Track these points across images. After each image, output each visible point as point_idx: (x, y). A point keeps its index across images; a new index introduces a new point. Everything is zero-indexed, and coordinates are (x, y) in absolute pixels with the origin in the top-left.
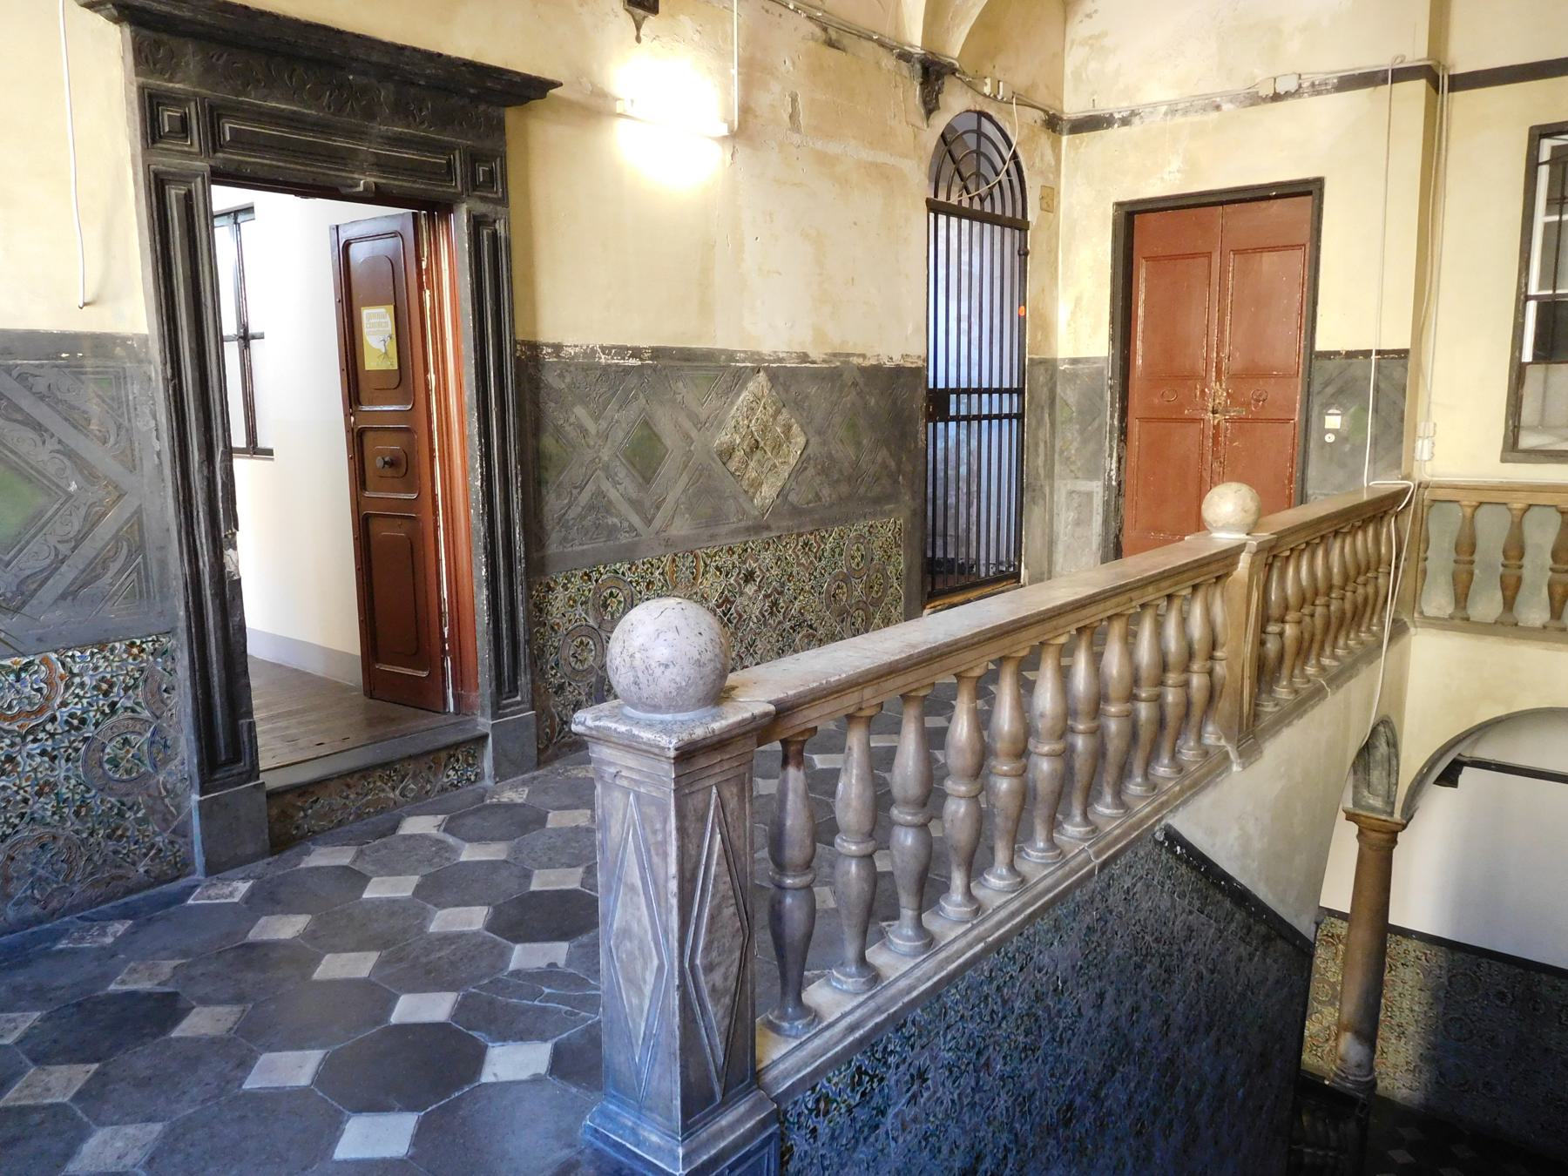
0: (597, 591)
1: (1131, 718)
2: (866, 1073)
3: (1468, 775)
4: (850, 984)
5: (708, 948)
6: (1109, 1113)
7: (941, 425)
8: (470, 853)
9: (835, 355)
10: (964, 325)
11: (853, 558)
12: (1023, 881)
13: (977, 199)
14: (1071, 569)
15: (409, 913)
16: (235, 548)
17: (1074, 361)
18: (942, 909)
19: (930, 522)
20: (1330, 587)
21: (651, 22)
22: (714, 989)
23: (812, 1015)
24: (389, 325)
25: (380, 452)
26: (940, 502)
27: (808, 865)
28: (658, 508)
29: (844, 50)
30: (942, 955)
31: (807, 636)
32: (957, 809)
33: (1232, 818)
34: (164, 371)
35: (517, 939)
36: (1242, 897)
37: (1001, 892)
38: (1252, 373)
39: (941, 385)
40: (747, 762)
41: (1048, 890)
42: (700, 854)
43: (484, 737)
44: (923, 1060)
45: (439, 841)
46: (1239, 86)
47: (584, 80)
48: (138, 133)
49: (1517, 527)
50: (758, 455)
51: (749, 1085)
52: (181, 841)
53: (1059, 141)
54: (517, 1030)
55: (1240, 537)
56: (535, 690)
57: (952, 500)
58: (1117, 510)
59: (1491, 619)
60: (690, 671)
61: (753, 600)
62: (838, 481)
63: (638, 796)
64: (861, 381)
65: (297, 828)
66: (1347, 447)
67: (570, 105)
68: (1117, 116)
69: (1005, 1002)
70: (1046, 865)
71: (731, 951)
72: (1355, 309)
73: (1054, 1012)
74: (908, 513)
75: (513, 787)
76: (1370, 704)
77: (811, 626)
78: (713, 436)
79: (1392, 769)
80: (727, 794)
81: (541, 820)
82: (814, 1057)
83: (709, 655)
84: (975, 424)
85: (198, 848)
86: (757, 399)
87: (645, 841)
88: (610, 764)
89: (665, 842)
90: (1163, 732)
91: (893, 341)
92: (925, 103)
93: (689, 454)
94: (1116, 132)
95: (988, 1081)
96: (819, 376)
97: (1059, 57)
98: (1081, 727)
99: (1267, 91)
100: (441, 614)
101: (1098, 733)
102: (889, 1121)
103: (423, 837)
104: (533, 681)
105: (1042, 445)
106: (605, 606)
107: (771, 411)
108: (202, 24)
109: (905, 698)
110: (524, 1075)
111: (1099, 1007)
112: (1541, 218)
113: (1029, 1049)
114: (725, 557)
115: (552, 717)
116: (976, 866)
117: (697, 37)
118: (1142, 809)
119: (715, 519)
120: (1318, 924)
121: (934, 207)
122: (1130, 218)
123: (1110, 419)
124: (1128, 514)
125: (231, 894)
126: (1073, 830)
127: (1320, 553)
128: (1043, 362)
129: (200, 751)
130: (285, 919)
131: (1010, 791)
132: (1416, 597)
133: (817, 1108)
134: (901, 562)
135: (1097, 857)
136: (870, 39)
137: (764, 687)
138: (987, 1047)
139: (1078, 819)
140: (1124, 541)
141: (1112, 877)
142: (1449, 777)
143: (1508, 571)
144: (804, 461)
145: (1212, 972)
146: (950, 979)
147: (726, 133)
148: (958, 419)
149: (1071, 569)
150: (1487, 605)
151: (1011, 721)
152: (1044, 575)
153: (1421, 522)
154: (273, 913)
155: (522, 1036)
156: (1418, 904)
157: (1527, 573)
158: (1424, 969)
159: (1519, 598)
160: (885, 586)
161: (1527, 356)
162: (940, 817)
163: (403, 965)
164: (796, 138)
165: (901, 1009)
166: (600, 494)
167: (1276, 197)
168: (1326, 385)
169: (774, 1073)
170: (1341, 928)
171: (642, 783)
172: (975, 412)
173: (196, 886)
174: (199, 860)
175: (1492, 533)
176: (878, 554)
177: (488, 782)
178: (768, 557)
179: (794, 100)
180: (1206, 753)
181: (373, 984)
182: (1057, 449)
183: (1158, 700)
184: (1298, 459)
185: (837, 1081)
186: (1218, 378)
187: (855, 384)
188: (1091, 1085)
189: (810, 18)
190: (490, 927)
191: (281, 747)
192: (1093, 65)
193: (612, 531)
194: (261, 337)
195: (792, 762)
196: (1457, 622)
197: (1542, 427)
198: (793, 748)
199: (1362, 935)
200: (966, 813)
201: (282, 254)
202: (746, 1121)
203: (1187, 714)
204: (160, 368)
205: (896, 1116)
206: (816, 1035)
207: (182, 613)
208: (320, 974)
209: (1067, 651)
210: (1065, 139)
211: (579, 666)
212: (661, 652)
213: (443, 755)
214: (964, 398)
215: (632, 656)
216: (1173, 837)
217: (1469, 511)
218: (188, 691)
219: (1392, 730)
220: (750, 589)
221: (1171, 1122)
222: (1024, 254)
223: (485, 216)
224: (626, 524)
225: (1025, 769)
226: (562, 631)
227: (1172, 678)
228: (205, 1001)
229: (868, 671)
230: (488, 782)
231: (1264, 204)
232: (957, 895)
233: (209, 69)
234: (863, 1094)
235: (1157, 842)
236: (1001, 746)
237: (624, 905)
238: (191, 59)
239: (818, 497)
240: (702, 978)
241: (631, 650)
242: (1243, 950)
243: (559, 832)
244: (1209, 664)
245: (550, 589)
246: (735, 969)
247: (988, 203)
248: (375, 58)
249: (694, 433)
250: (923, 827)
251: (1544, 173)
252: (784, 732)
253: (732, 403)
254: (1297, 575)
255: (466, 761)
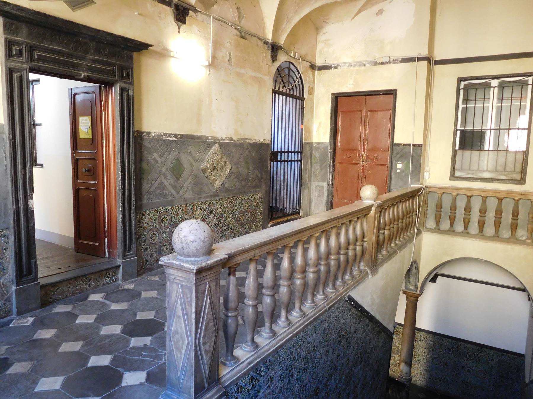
0: (160, 216)
1: (338, 260)
2: (254, 378)
3: (439, 279)
4: (249, 348)
5: (204, 337)
6: (330, 390)
7: (275, 163)
8: (114, 307)
9: (241, 139)
10: (283, 130)
11: (246, 206)
12: (304, 314)
13: (288, 90)
14: (317, 213)
15: (93, 328)
16: (32, 199)
17: (318, 143)
18: (278, 323)
19: (271, 195)
20: (399, 219)
21: (183, 27)
22: (206, 351)
23: (236, 359)
24: (89, 123)
25: (85, 167)
26: (275, 188)
27: (236, 309)
28: (181, 188)
29: (246, 40)
30: (279, 338)
31: (230, 232)
32: (284, 290)
33: (369, 292)
34: (9, 137)
35: (133, 336)
36: (372, 318)
37: (297, 317)
38: (375, 150)
39: (276, 150)
40: (218, 274)
41: (312, 317)
42: (203, 305)
43: (119, 266)
44: (272, 374)
45: (102, 303)
46: (371, 59)
47: (160, 44)
48: (4, 54)
49: (454, 201)
50: (215, 171)
51: (216, 383)
52: (8, 303)
53: (315, 73)
54: (134, 368)
55: (372, 202)
56: (138, 251)
57: (278, 188)
58: (332, 192)
59: (446, 229)
60: (201, 244)
61: (212, 220)
62: (241, 181)
63: (182, 286)
64: (250, 148)
65: (51, 298)
66: (404, 174)
67: (156, 53)
68: (333, 66)
69: (298, 354)
70: (312, 308)
71: (212, 338)
72: (405, 133)
73: (313, 357)
74: (264, 191)
75: (129, 283)
76: (411, 257)
77: (231, 229)
78: (200, 165)
79: (417, 278)
80: (212, 285)
81: (139, 295)
82: (237, 373)
83: (207, 239)
84: (286, 163)
85: (14, 306)
86: (215, 153)
87: (184, 301)
88: (172, 275)
89: (191, 301)
90: (345, 267)
91: (260, 134)
92: (272, 58)
93: (192, 171)
94: (332, 71)
95: (293, 380)
96: (235, 145)
97: (315, 46)
98: (323, 263)
99: (379, 61)
100: (104, 223)
101: (328, 265)
102: (261, 394)
103: (97, 301)
104: (137, 247)
105: (308, 170)
106: (162, 221)
107: (220, 156)
108: (29, 18)
109: (268, 253)
110: (137, 383)
111: (327, 355)
112: (461, 106)
113: (306, 369)
114: (203, 205)
115: (143, 259)
116: (289, 309)
117: (198, 32)
118: (341, 290)
119: (200, 192)
120: (394, 327)
121: (275, 92)
122: (337, 98)
123: (329, 162)
124: (335, 193)
125: (27, 322)
126: (319, 297)
127: (396, 208)
128: (308, 143)
129: (17, 271)
130: (47, 331)
131: (301, 284)
132: (424, 222)
133: (238, 391)
134: (261, 208)
135: (327, 305)
136: (255, 36)
137: (225, 248)
138: (292, 369)
139: (321, 293)
140: (334, 202)
141: (332, 312)
142: (434, 280)
143: (452, 214)
144: (230, 174)
145: (362, 343)
146: (281, 347)
147: (207, 64)
148: (281, 161)
149: (317, 213)
150: (445, 225)
151: (301, 261)
152: (308, 214)
153: (426, 198)
154: (44, 329)
155: (136, 369)
156: (425, 321)
157: (457, 215)
158: (426, 341)
159: (455, 223)
160: (256, 216)
161: (457, 148)
162: (278, 293)
163: (92, 346)
164: (230, 67)
165: (265, 356)
166: (161, 183)
167: (382, 94)
168: (397, 154)
169: (224, 379)
170: (401, 329)
171: (184, 281)
172: (286, 159)
173: (13, 320)
174: (14, 310)
175: (447, 202)
176: (254, 205)
177: (120, 282)
178: (218, 205)
179: (230, 55)
180: (361, 272)
181: (81, 353)
182: (312, 172)
183: (346, 254)
184: (389, 177)
185: (245, 381)
186: (364, 151)
187: (248, 149)
188: (324, 382)
189: (236, 29)
190: (123, 332)
191: (46, 270)
192: (326, 49)
193: (165, 196)
194: (40, 125)
195: (232, 274)
196: (437, 230)
197: (461, 170)
198: (232, 270)
199: (408, 331)
200: (287, 291)
201: (51, 97)
202: (216, 395)
203: (355, 259)
204: (8, 136)
205: (263, 393)
206: (238, 366)
207: (12, 222)
208: (62, 349)
209: (318, 238)
210: (316, 72)
211: (152, 242)
212: (191, 238)
213: (104, 272)
214: (283, 154)
215: (181, 239)
216: (351, 299)
217: (440, 195)
218: (13, 250)
219: (417, 265)
220: (212, 216)
221: (349, 393)
222: (303, 108)
223: (125, 88)
224: (170, 193)
225: (305, 277)
226: (147, 229)
227: (351, 247)
228: (18, 360)
229: (257, 245)
230: (120, 282)
231: (378, 96)
232: (283, 318)
233: (30, 34)
234: (253, 386)
235: (346, 301)
236: (298, 269)
237: (176, 322)
238: (24, 30)
239: (235, 186)
240: (202, 346)
241: (181, 237)
242: (371, 336)
243: (146, 299)
244: (362, 243)
245: (144, 215)
246: (213, 344)
247: (292, 91)
248: (90, 33)
249: (194, 163)
250: (273, 296)
251: (462, 92)
252: (229, 265)
253: (207, 154)
254: (389, 214)
255: (112, 274)
